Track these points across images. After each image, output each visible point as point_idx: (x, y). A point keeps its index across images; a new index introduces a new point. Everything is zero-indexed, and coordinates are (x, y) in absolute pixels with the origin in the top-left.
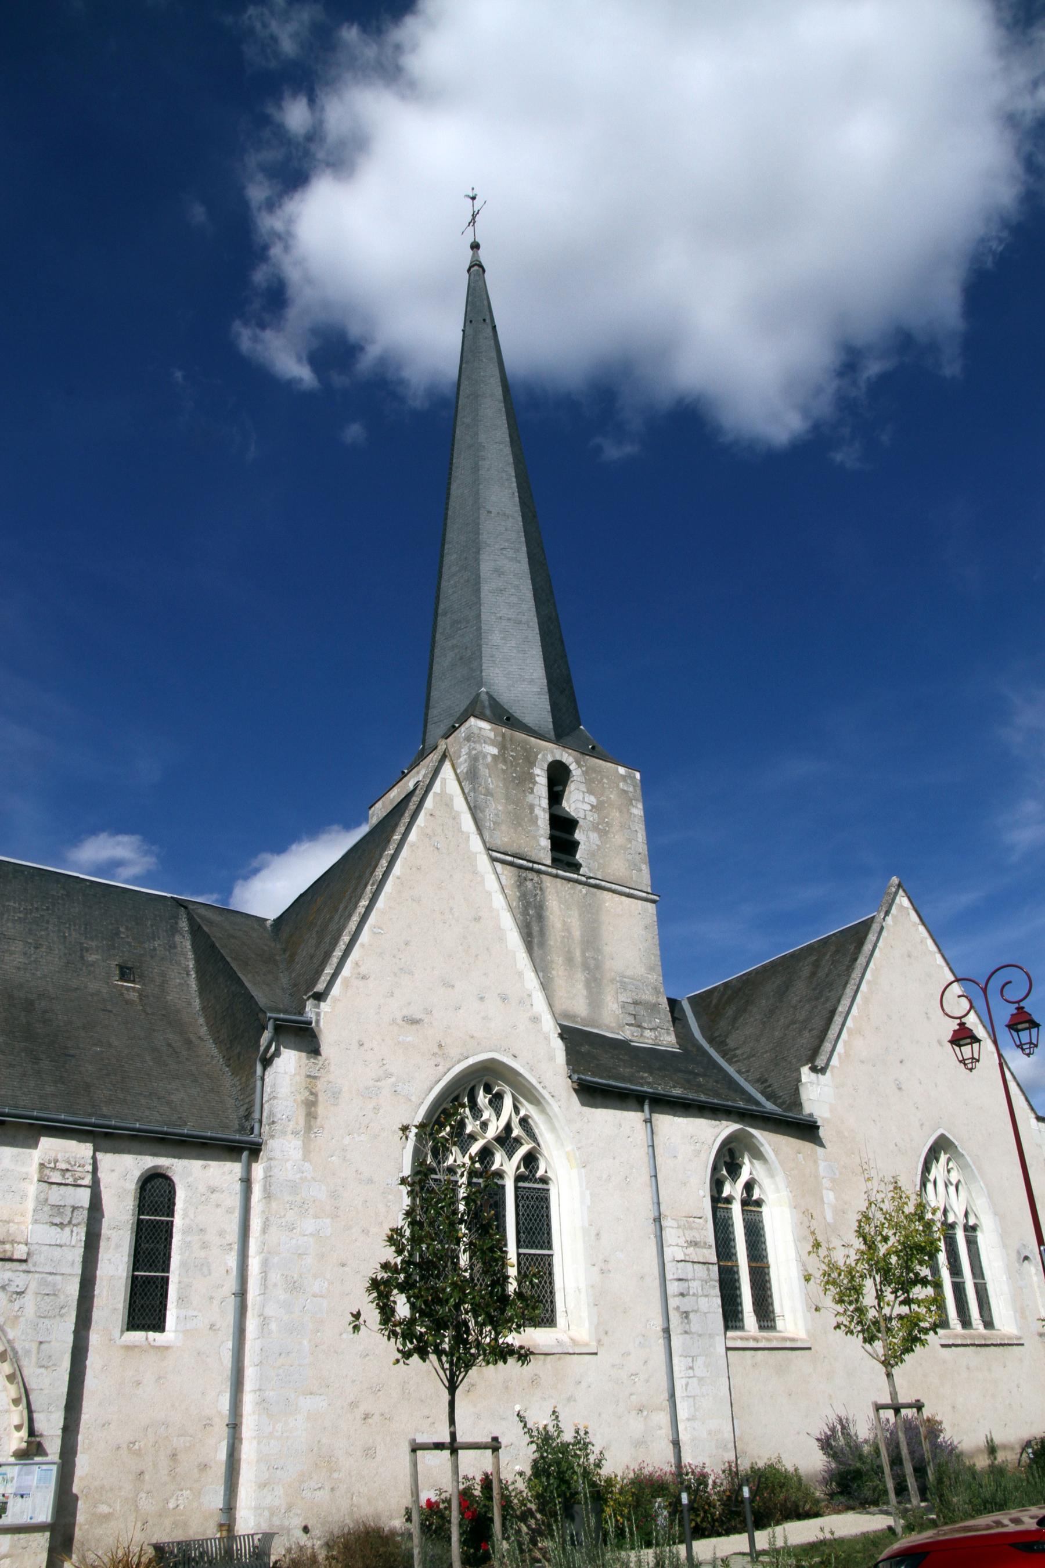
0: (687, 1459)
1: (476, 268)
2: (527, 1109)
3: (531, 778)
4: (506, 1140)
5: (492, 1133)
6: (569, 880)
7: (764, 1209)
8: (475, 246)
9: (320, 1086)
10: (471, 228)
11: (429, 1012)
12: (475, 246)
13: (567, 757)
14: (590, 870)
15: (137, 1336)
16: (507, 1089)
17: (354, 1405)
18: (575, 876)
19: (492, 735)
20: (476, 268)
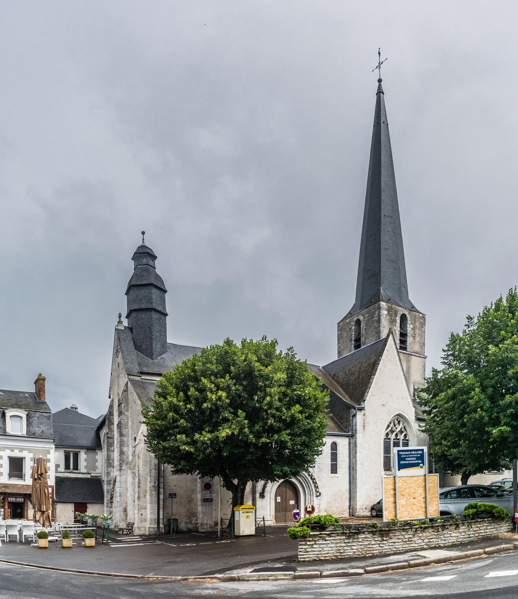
0: (398, 517)
1: (380, 92)
2: (405, 424)
3: (395, 321)
4: (401, 432)
5: (398, 430)
6: (404, 353)
7: (46, 382)
8: (380, 81)
9: (366, 422)
10: (377, 70)
11: (387, 403)
12: (380, 81)
13: (406, 313)
14: (410, 349)
15: (333, 475)
16: (401, 419)
17: (373, 487)
18: (405, 352)
19: (386, 307)
20: (380, 92)
